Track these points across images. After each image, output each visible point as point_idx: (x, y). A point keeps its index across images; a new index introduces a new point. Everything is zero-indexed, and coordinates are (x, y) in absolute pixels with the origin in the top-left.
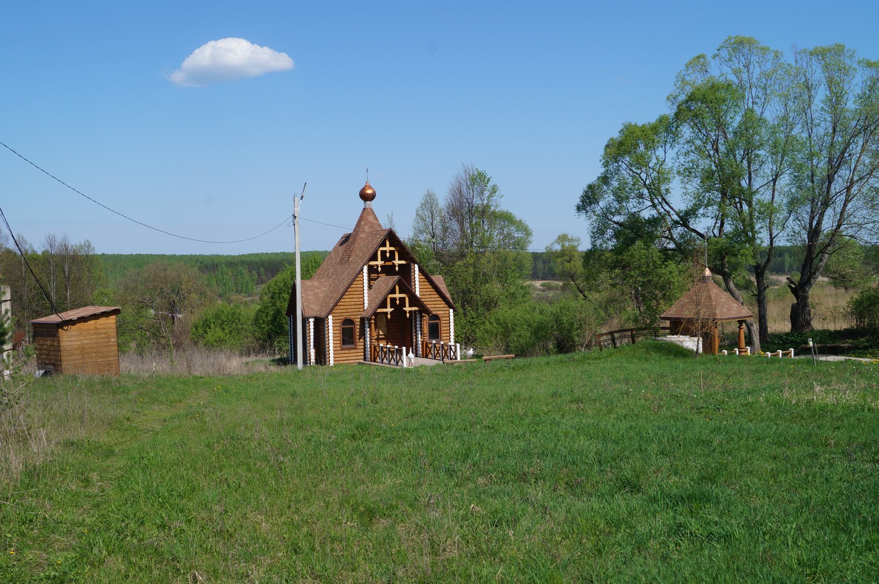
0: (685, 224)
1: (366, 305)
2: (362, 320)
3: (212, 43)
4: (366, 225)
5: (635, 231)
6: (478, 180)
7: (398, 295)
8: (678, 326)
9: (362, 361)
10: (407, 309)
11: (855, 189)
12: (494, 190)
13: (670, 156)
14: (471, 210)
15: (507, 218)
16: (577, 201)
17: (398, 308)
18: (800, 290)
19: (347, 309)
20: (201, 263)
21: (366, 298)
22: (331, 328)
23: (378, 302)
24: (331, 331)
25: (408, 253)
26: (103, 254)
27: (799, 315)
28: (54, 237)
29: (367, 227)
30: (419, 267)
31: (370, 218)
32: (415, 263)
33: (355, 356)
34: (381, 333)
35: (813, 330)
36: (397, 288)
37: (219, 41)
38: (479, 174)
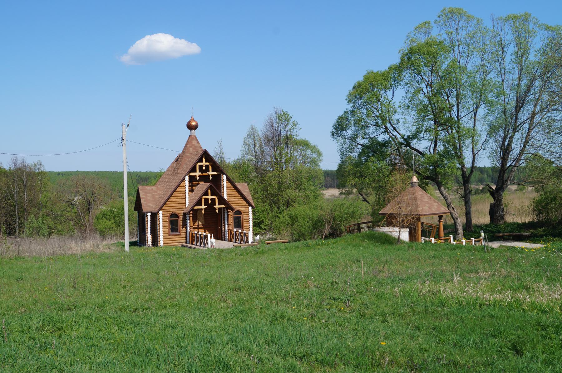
0: (408, 144)
1: (187, 204)
2: (185, 214)
3: (148, 37)
4: (191, 147)
5: (375, 149)
6: (283, 118)
7: (210, 197)
8: (390, 221)
9: (184, 244)
10: (217, 206)
11: (537, 118)
12: (294, 125)
13: (398, 96)
14: (279, 139)
15: (305, 144)
16: (332, 129)
17: (210, 205)
18: (496, 194)
19: (174, 207)
20: (139, 176)
21: (187, 199)
22: (161, 220)
23: (195, 201)
24: (161, 222)
25: (218, 167)
26: (77, 171)
27: (496, 211)
28: (16, 158)
29: (191, 149)
30: (227, 177)
31: (194, 142)
32: (224, 174)
33: (179, 240)
34: (200, 223)
35: (505, 222)
36: (209, 191)
37: (153, 36)
38: (284, 113)
